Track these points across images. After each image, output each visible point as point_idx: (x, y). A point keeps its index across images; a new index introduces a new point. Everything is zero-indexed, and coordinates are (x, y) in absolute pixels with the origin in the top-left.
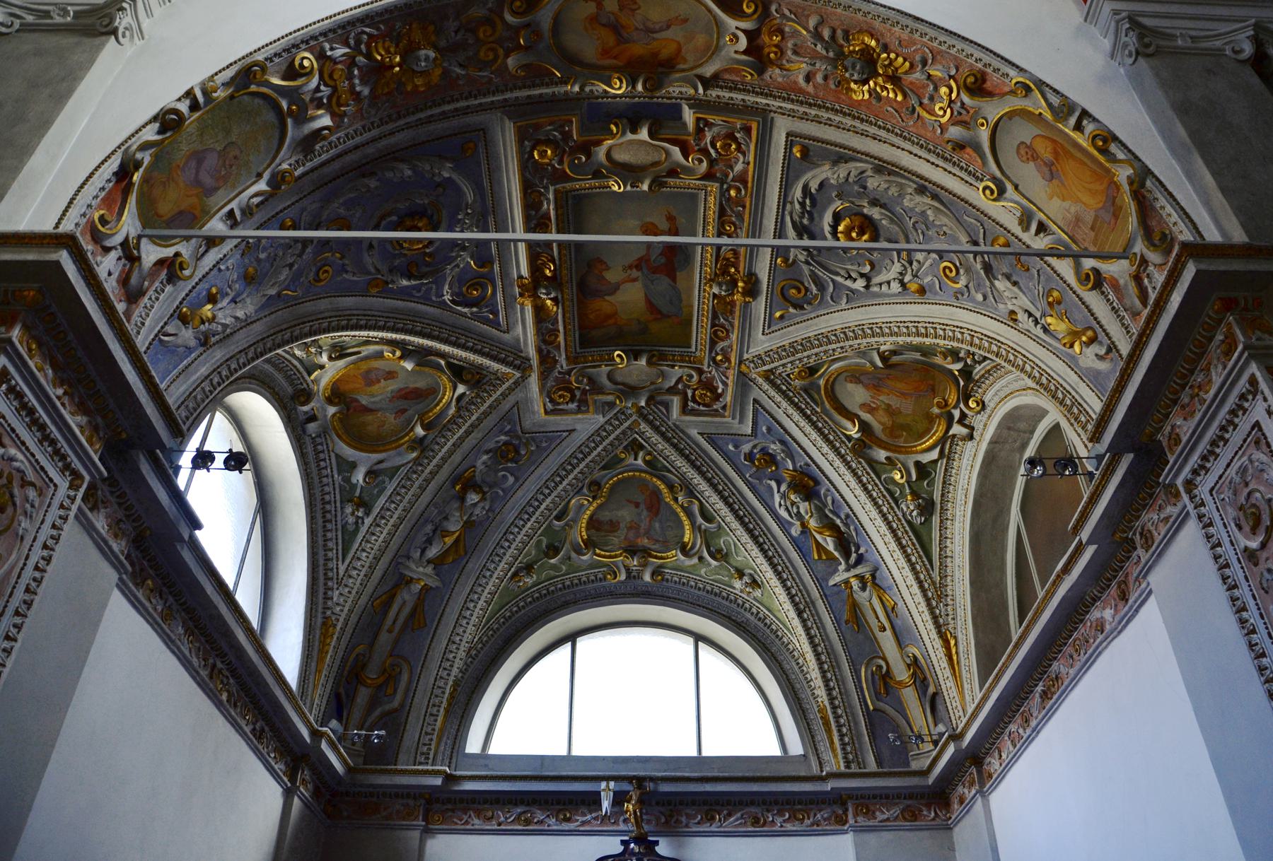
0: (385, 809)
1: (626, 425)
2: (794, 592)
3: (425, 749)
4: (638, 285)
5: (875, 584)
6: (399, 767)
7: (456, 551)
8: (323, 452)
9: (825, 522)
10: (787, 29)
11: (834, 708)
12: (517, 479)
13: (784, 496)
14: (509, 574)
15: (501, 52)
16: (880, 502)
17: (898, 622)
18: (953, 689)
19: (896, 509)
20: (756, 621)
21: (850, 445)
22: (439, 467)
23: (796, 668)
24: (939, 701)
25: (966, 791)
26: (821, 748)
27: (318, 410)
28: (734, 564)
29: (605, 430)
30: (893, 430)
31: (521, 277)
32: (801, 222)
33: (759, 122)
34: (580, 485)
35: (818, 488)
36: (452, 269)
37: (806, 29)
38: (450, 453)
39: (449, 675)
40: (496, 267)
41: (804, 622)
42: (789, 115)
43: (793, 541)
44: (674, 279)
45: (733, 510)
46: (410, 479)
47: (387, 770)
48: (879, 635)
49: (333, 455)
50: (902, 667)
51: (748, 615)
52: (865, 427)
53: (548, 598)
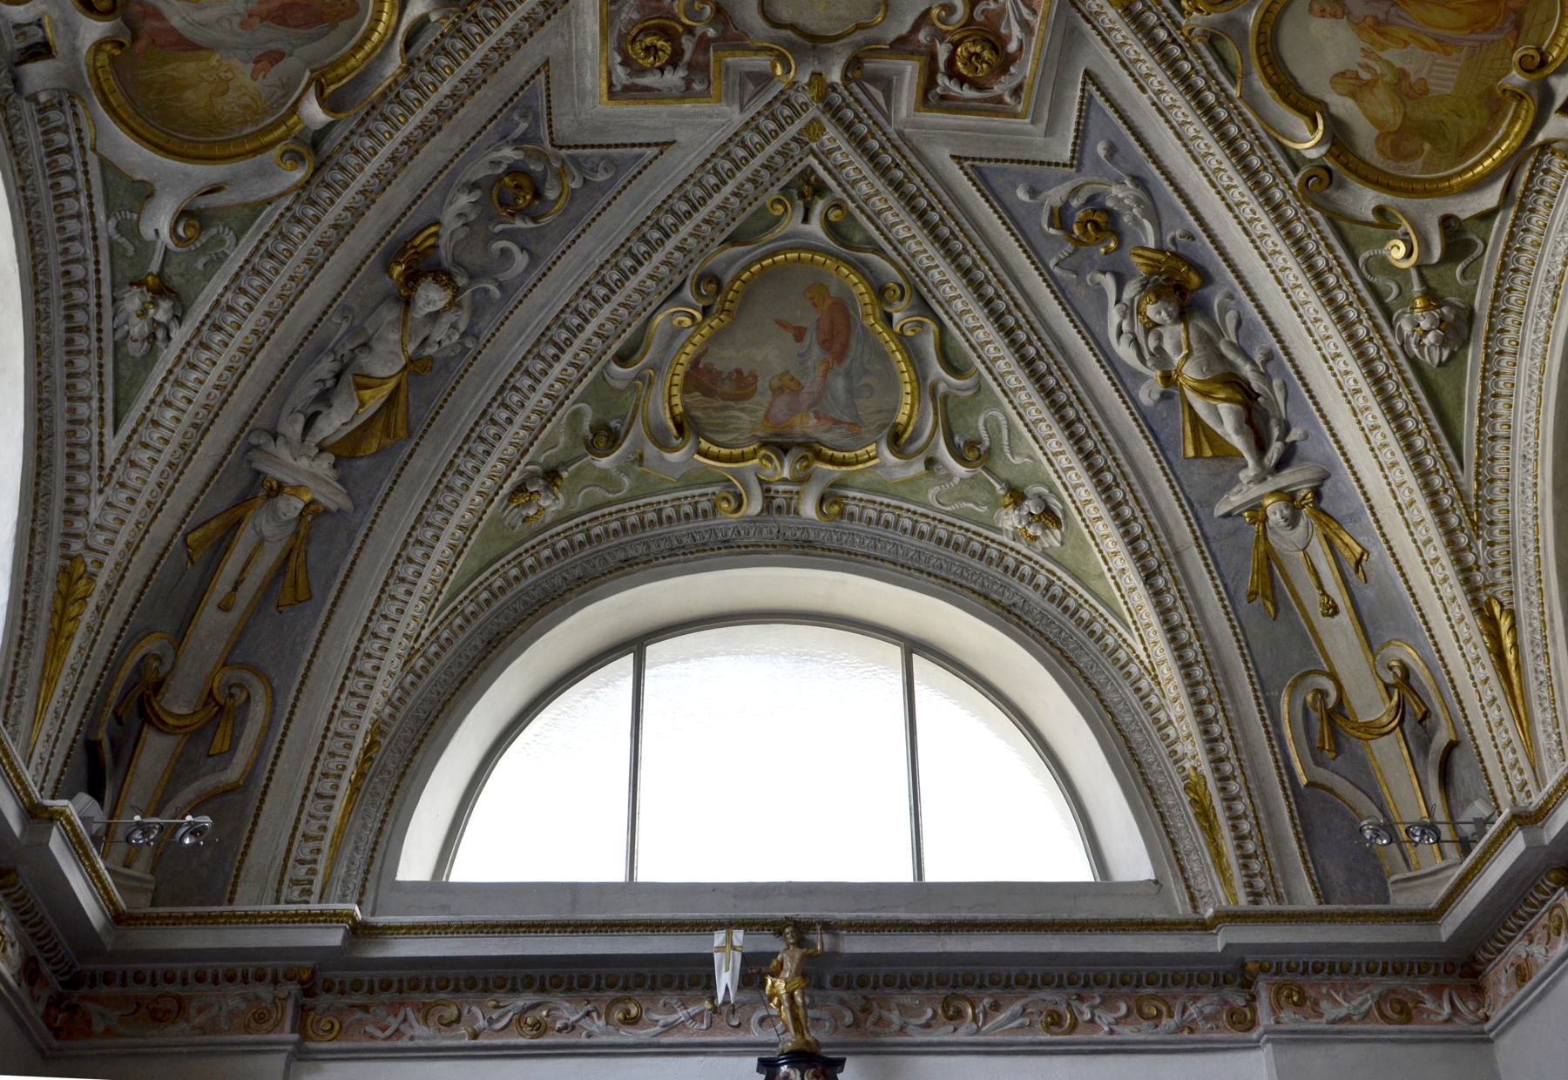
0: (200, 1011)
1: (792, 130)
2: (1137, 530)
3: (302, 872)
5: (1320, 513)
6: (239, 908)
7: (387, 430)
8: (67, 150)
9: (1219, 369)
11: (1223, 779)
12: (534, 259)
13: (1130, 311)
14: (507, 487)
16: (1352, 315)
17: (1367, 594)
18: (1508, 723)
19: (1387, 331)
20: (1046, 604)
21: (1295, 181)
22: (357, 213)
23: (1134, 699)
24: (1459, 759)
25: (1538, 950)
26: (1193, 866)
27: (53, 23)
28: (1004, 474)
29: (743, 145)
30: (1398, 141)
34: (678, 279)
35: (1206, 291)
38: (385, 180)
39: (362, 707)
41: (1157, 594)
43: (1143, 417)
45: (1017, 348)
46: (284, 237)
47: (209, 915)
48: (1322, 623)
49: (93, 160)
50: (1374, 691)
51: (1028, 591)
52: (1338, 135)
53: (588, 550)
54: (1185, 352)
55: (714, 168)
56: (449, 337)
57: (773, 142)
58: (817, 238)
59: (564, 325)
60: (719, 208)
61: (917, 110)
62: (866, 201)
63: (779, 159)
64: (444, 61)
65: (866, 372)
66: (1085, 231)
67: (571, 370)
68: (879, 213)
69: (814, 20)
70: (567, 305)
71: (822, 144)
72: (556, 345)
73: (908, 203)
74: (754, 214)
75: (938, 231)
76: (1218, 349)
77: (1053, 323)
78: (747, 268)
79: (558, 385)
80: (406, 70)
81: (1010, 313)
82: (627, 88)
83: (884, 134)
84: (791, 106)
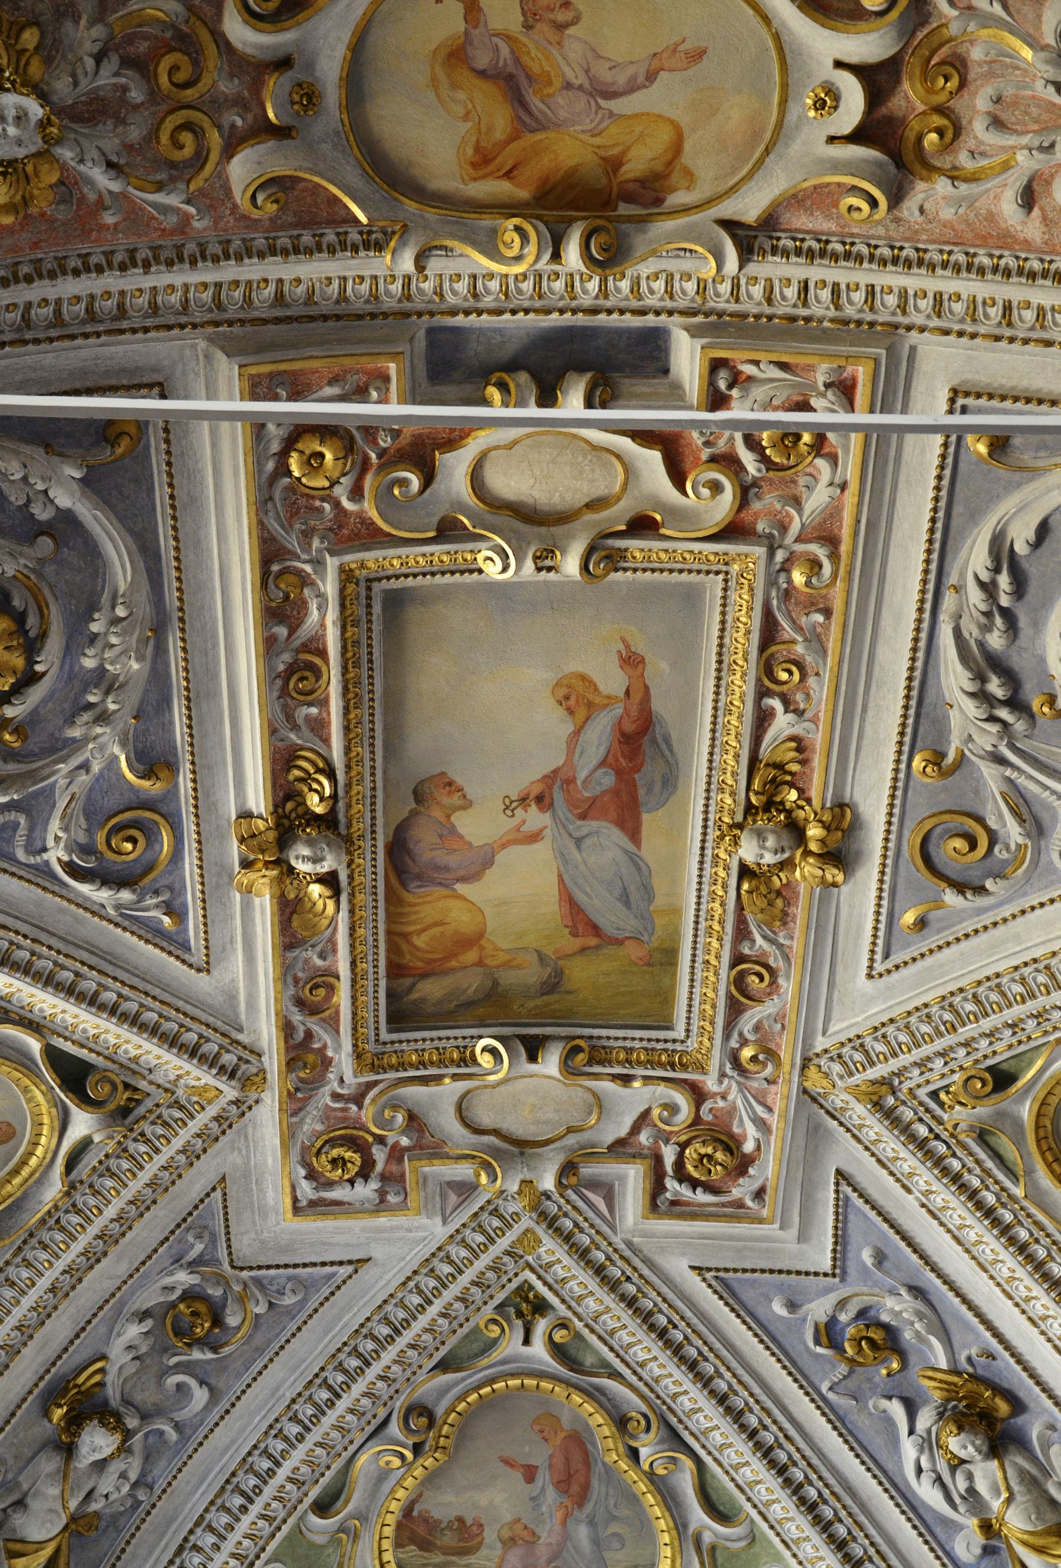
1: (504, 1243)
4: (542, 850)
10: (976, 54)
12: (215, 1395)
13: (929, 1444)
15: (215, 139)
31: (246, 815)
32: (981, 644)
33: (876, 361)
34: (382, 1413)
35: (1020, 1420)
36: (72, 774)
37: (1032, 43)
40: (184, 782)
42: (961, 334)
44: (634, 835)
54: (1005, 1495)
55: (417, 1286)
56: (118, 1489)
57: (483, 1256)
58: (540, 1361)
59: (251, 1470)
60: (426, 1330)
61: (645, 1217)
62: (595, 1319)
63: (490, 1275)
64: (109, 1183)
65: (614, 1518)
66: (860, 1351)
67: (261, 1523)
68: (612, 1333)
69: (520, 1126)
70: (255, 1447)
71: (539, 1258)
72: (243, 1493)
73: (645, 1321)
74: (467, 1336)
75: (699, 1368)
76: (1046, 1492)
77: (834, 1458)
78: (462, 1397)
79: (246, 1543)
80: (68, 1194)
81: (780, 1446)
82: (313, 1204)
83: (610, 1244)
84: (501, 1217)
